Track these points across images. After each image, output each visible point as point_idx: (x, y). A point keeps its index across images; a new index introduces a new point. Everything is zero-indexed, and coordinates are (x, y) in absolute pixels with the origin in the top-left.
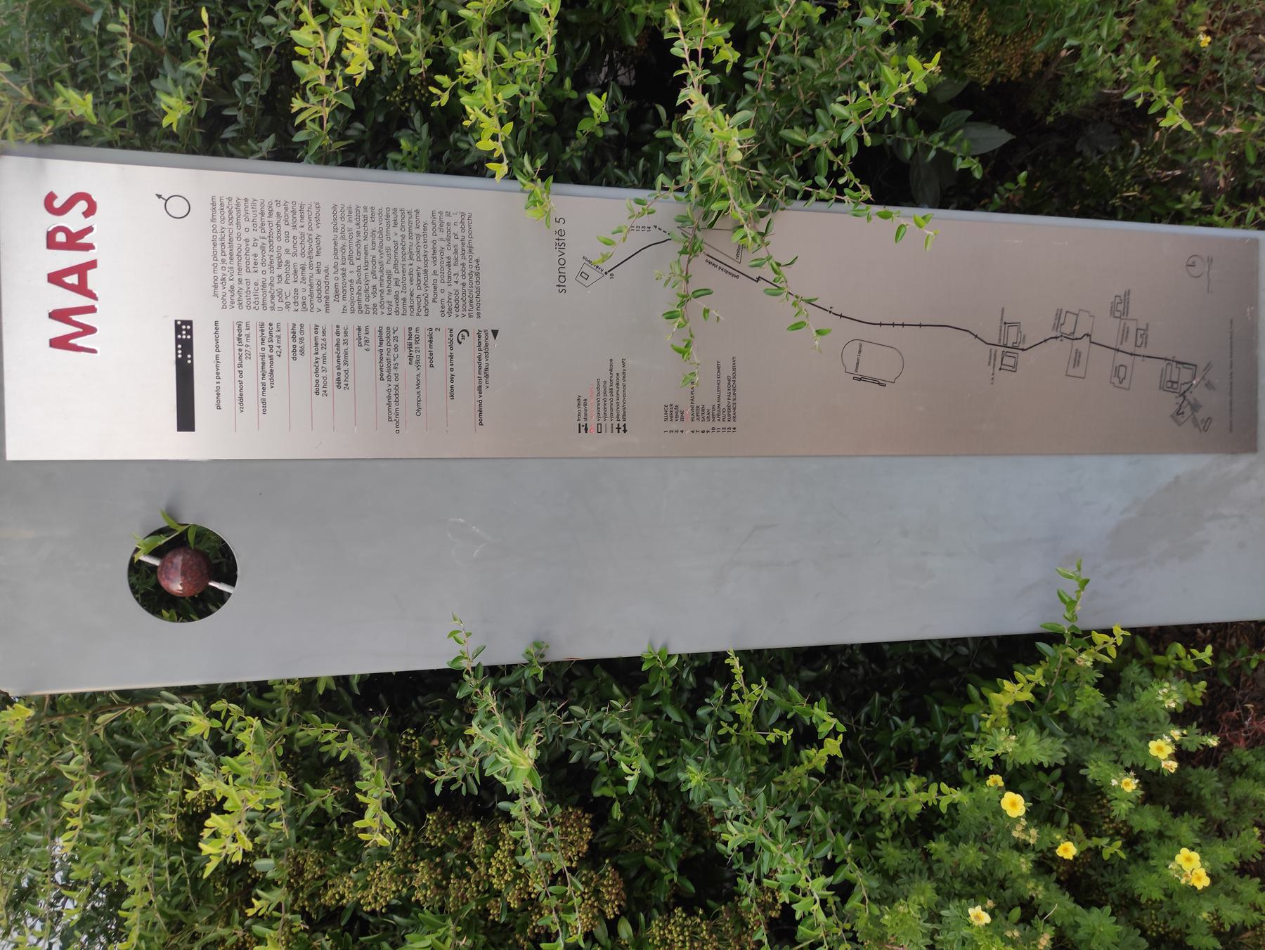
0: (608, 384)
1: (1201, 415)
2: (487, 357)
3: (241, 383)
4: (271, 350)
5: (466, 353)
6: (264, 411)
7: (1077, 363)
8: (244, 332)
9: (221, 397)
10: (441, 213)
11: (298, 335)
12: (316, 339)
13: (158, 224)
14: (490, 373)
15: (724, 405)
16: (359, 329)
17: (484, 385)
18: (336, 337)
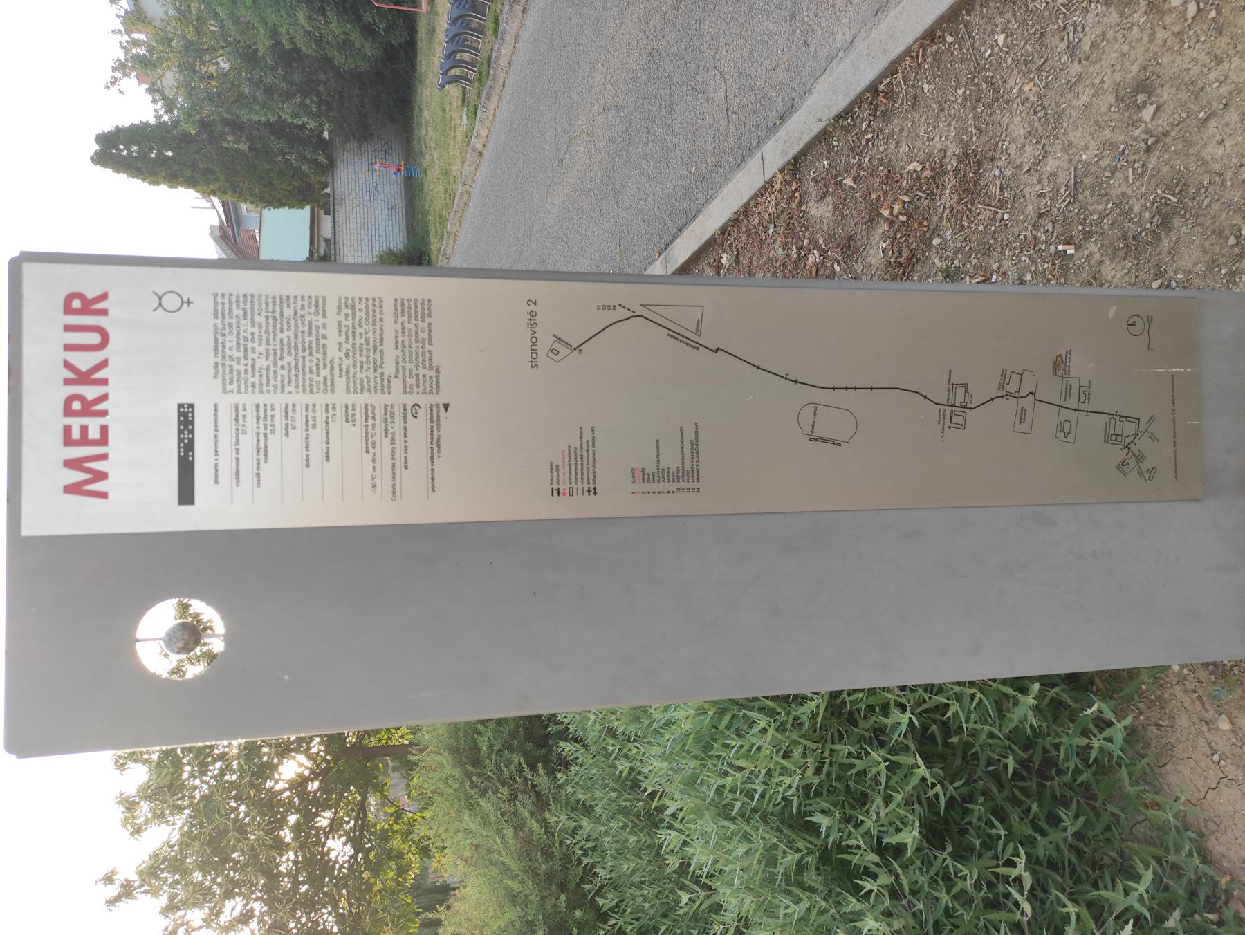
1: (1145, 466)
2: (439, 429)
3: (237, 460)
4: (266, 428)
5: (418, 428)
7: (1022, 419)
8: (241, 413)
11: (290, 414)
12: (307, 417)
15: (688, 466)
16: (347, 407)
17: (436, 455)
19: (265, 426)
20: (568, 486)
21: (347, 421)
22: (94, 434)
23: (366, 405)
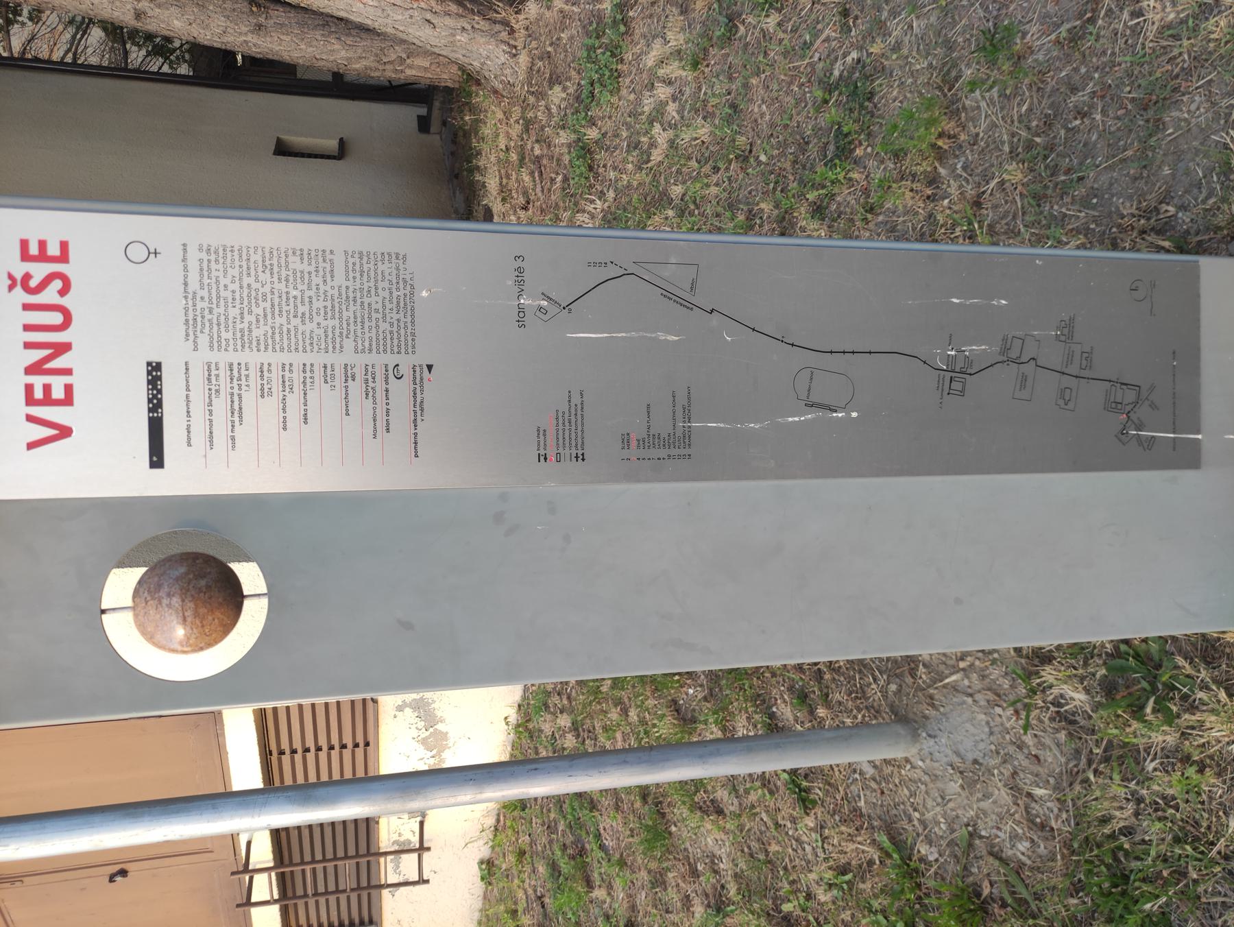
0: (567, 415)
2: (422, 391)
3: (211, 421)
4: (240, 389)
6: (233, 447)
7: (1023, 386)
8: (214, 372)
9: (192, 435)
10: (324, 251)
13: (139, 272)
14: (425, 406)
16: (325, 367)
18: (302, 375)
21: (326, 382)
22: (58, 393)
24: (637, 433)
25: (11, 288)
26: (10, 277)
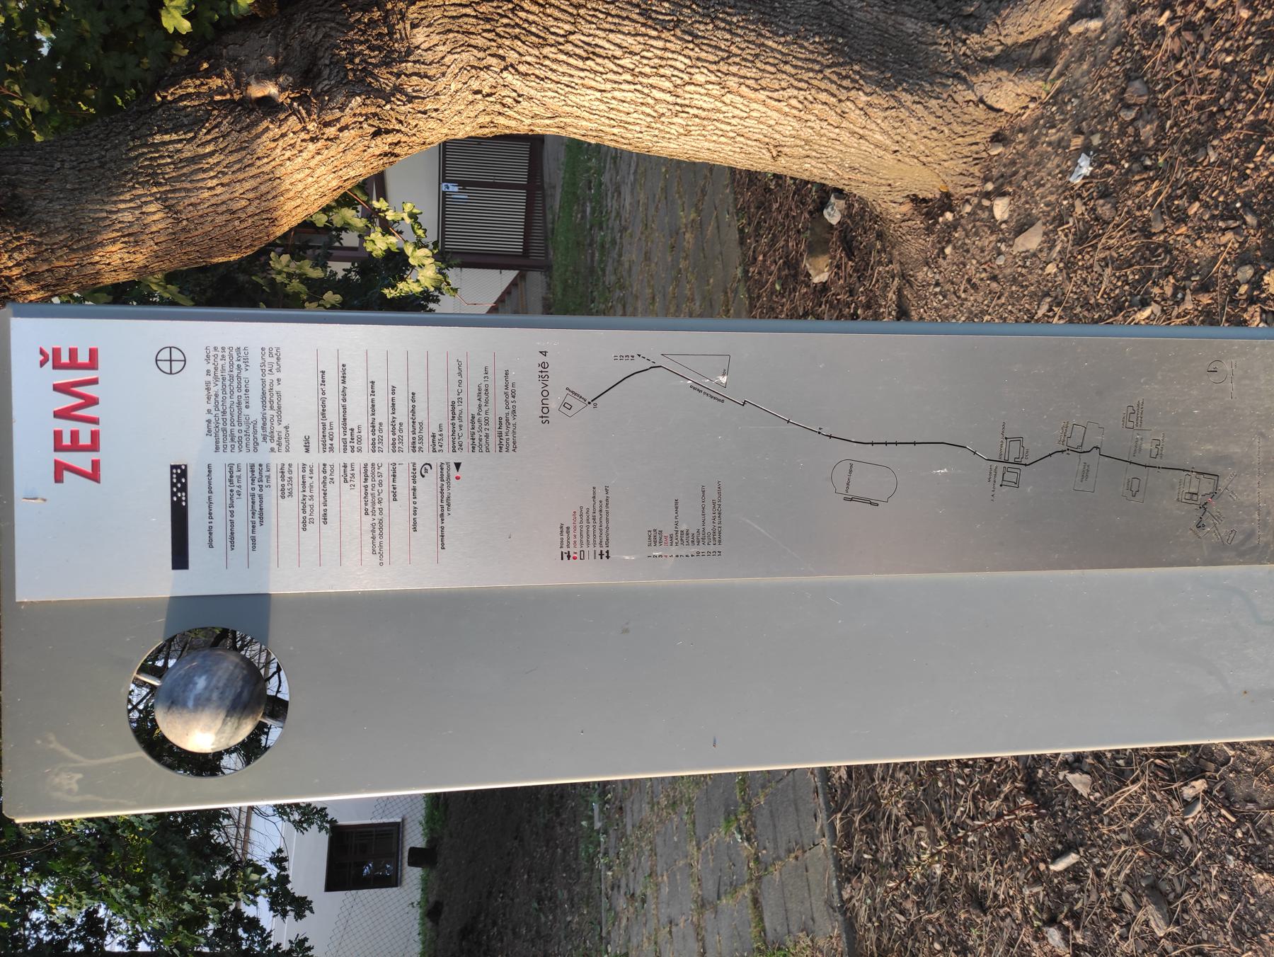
3: (232, 522)
4: (261, 490)
8: (236, 473)
11: (287, 475)
15: (709, 529)
16: (345, 466)
17: (446, 512)
19: (261, 486)
20: (578, 550)
21: (346, 481)
22: (85, 439)
23: (366, 465)
24: (668, 530)
25: (42, 364)
26: (42, 352)
